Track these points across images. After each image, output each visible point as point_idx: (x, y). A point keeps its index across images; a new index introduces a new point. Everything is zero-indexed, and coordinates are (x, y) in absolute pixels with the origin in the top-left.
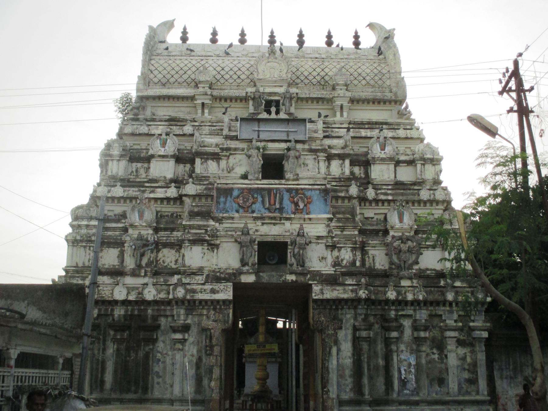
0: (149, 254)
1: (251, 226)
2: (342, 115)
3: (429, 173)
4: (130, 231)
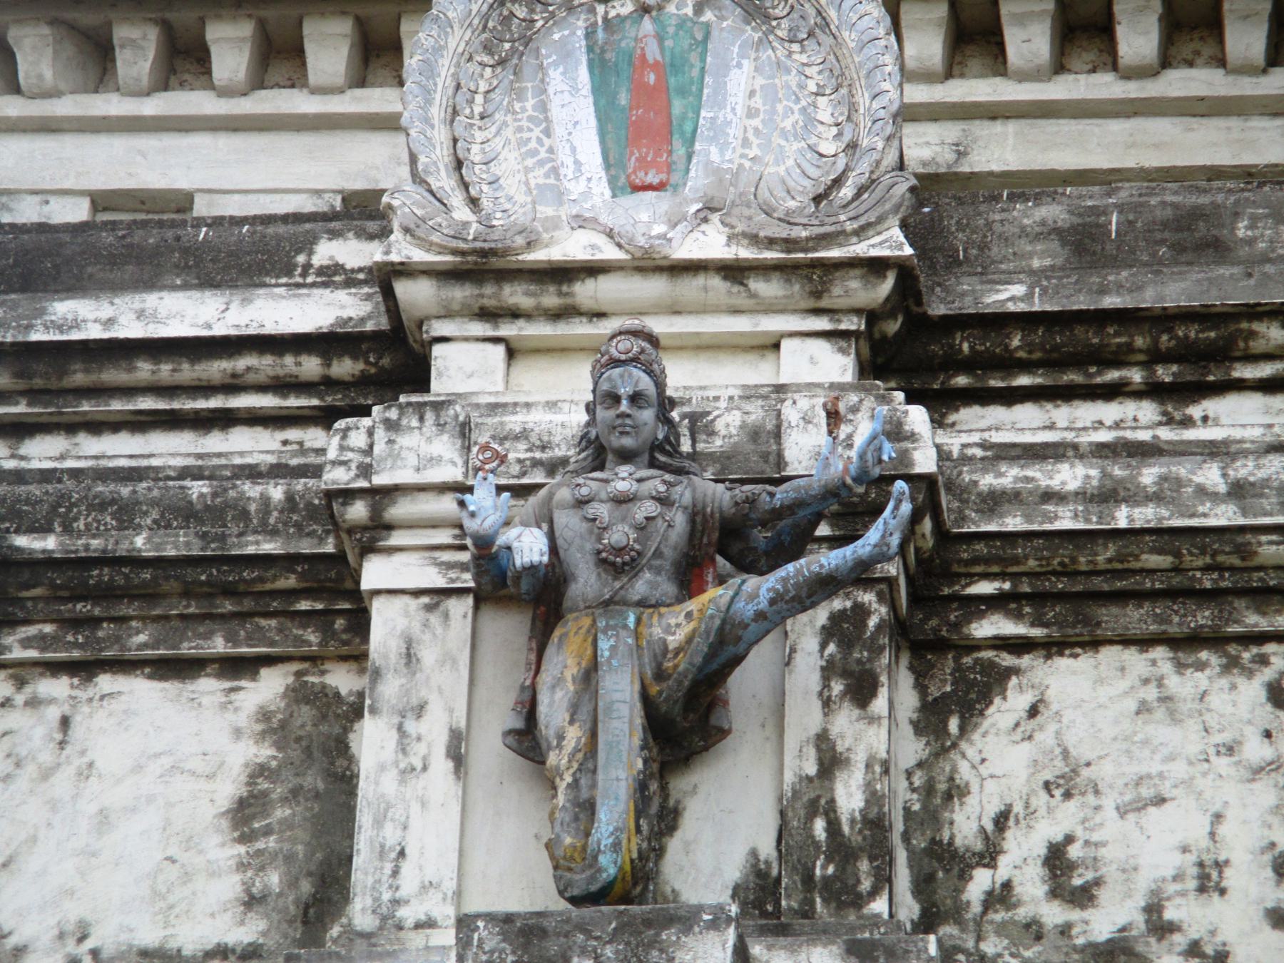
0: (804, 717)
4: (464, 365)
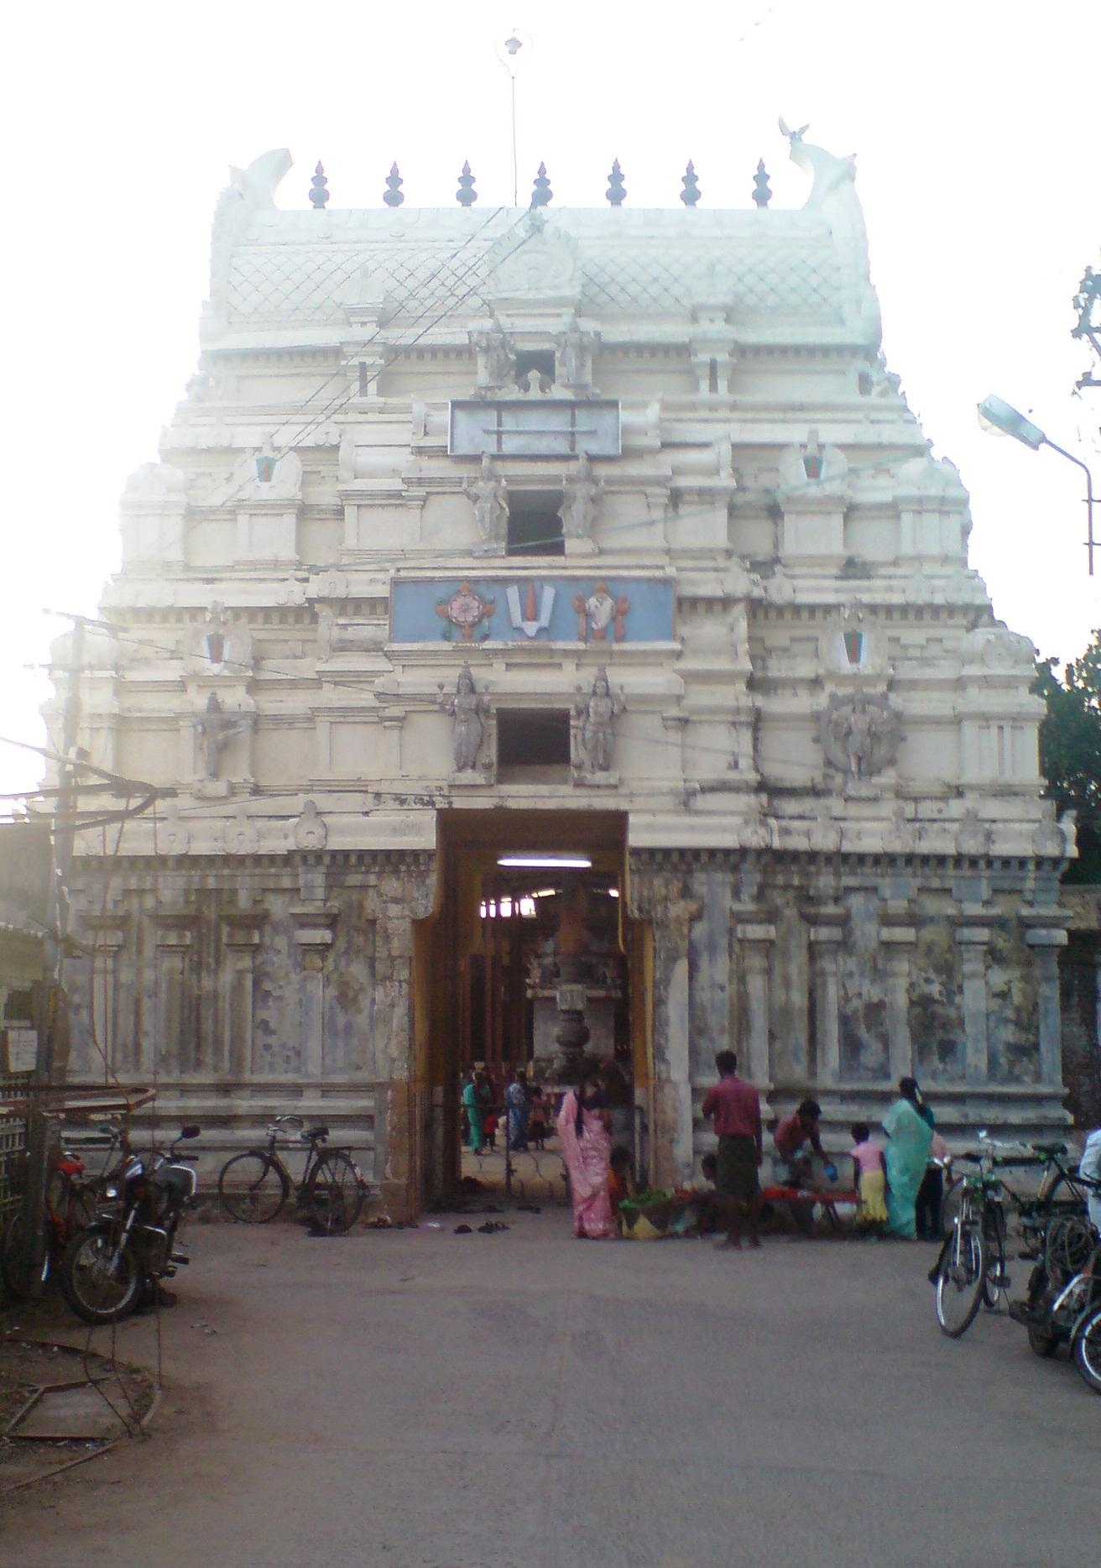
1: (480, 674)
2: (713, 387)
3: (927, 536)
